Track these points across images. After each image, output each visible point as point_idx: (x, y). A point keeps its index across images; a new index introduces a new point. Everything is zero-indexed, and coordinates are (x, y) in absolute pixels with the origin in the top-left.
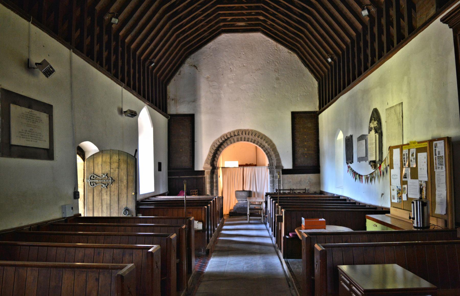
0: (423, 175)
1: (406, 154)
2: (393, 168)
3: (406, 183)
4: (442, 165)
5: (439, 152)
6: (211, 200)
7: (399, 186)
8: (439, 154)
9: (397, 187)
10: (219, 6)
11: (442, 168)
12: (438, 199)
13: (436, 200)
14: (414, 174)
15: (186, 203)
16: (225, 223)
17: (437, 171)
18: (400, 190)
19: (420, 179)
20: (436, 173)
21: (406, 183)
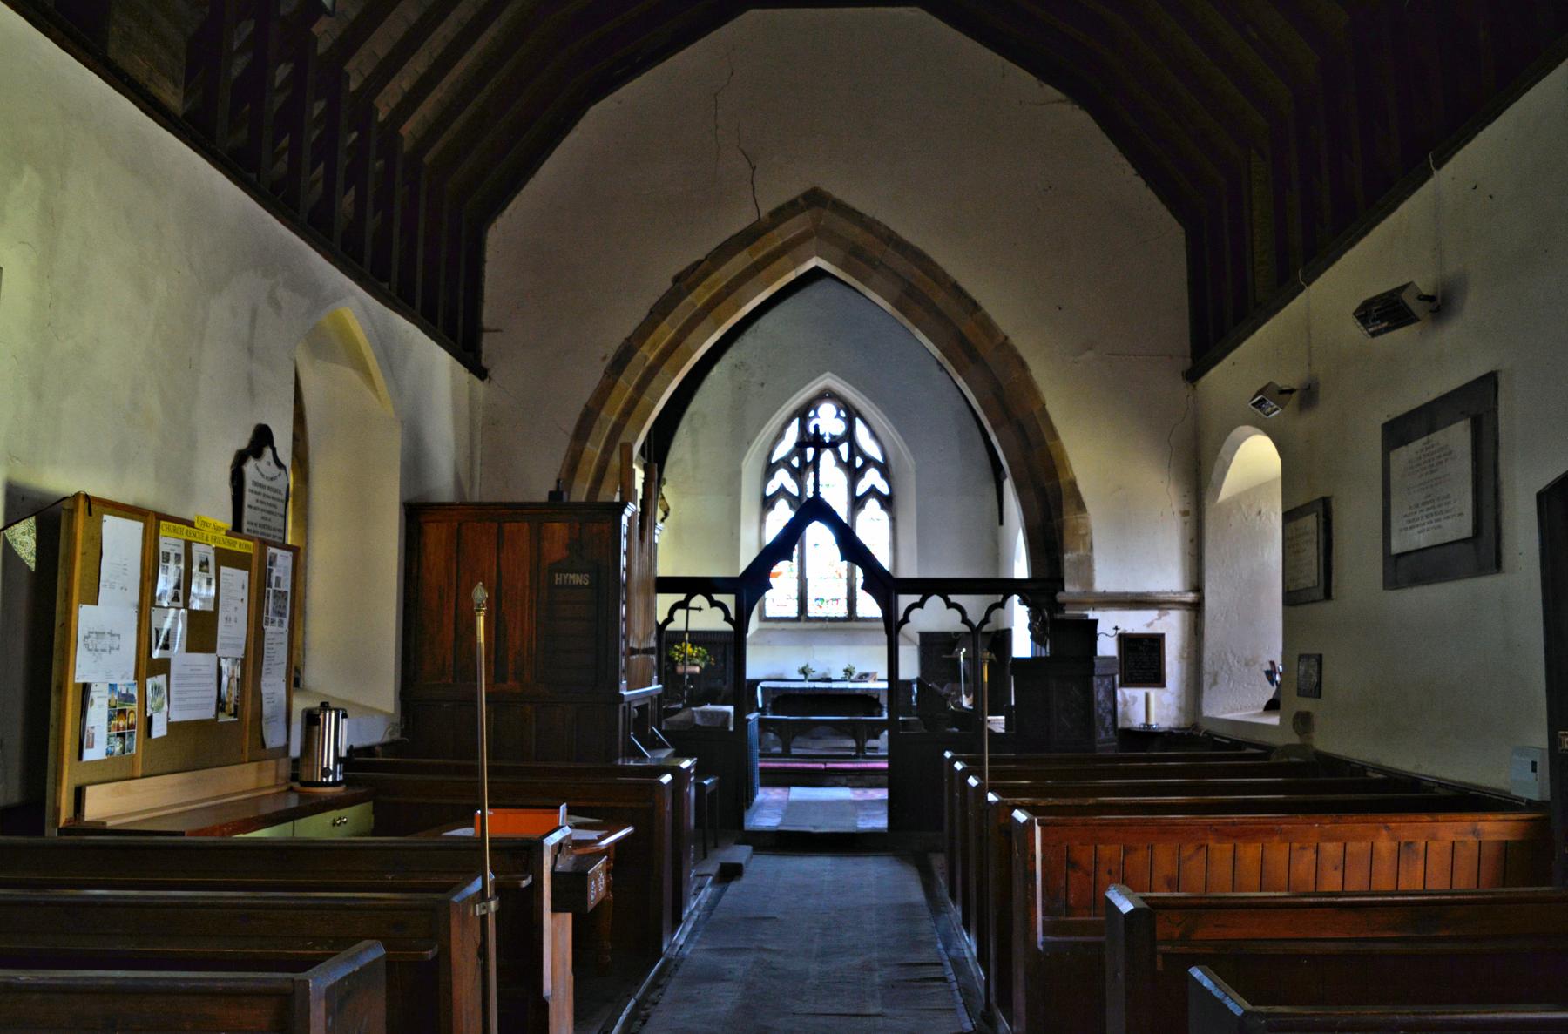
0: (232, 631)
1: (177, 556)
2: (95, 601)
3: (163, 667)
4: (282, 615)
5: (278, 579)
6: (664, 771)
7: (126, 682)
8: (278, 584)
9: (112, 687)
10: (637, 448)
11: (281, 623)
12: (267, 709)
13: (1212, 371)
14: (202, 631)
15: (476, 791)
16: (770, 808)
17: (269, 629)
18: (128, 698)
19: (220, 651)
20: (267, 636)
21: (163, 667)
